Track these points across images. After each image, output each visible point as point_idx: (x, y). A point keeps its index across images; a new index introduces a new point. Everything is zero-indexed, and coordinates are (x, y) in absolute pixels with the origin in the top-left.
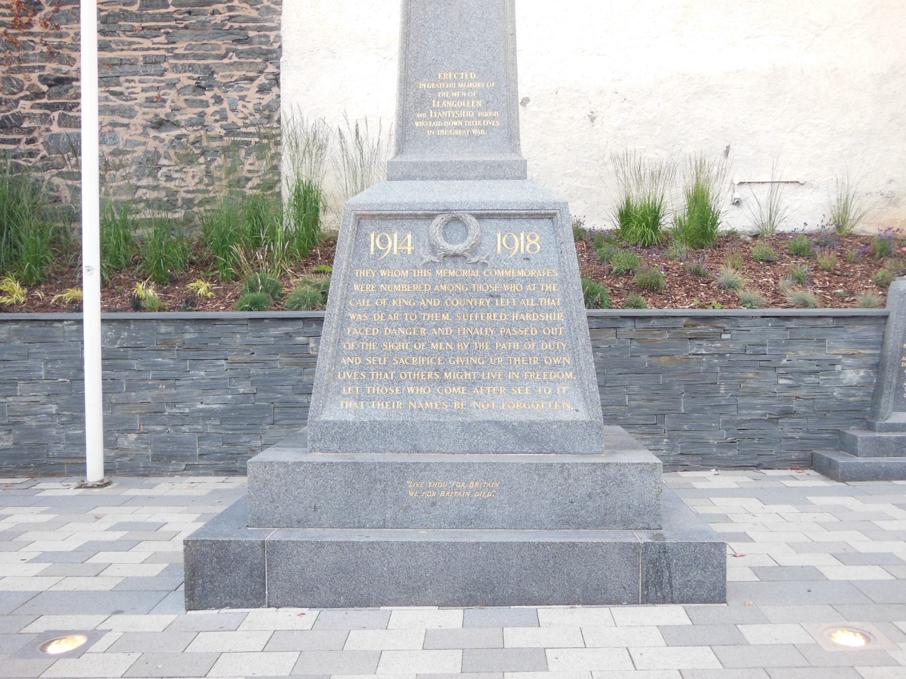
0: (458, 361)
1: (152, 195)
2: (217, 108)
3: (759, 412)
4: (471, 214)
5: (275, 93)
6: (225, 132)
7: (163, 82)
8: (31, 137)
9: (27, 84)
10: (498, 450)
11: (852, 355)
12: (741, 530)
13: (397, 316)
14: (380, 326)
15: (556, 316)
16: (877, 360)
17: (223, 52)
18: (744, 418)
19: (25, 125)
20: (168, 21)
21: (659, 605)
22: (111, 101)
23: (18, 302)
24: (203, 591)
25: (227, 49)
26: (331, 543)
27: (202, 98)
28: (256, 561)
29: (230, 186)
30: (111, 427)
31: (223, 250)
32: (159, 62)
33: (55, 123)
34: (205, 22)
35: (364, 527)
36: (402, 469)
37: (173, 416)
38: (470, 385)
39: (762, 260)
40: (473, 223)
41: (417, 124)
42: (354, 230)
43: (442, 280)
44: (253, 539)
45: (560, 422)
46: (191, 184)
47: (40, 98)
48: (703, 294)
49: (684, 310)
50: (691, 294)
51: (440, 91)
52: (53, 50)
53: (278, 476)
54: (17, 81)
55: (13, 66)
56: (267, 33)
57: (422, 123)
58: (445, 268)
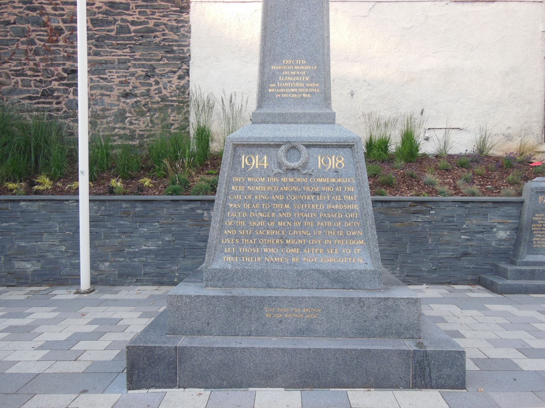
0: (294, 232)
1: (122, 132)
2: (156, 87)
4: (302, 144)
5: (187, 80)
6: (160, 99)
7: (128, 73)
8: (58, 101)
9: (56, 73)
10: (319, 287)
12: (455, 329)
14: (247, 211)
15: (354, 206)
16: (517, 226)
17: (160, 57)
18: (442, 256)
19: (55, 94)
21: (423, 390)
22: (101, 82)
23: (47, 189)
24: (138, 378)
25: (162, 56)
26: (218, 348)
27: (149, 81)
28: (171, 359)
29: (163, 128)
31: (158, 161)
32: (126, 63)
33: (71, 94)
35: (238, 335)
36: (262, 300)
37: (129, 253)
39: (443, 169)
41: (270, 90)
42: (232, 153)
44: (170, 346)
45: (356, 270)
46: (143, 126)
47: (63, 81)
48: (416, 188)
51: (284, 71)
53: (185, 304)
55: (48, 63)
57: (273, 90)
58: (287, 177)
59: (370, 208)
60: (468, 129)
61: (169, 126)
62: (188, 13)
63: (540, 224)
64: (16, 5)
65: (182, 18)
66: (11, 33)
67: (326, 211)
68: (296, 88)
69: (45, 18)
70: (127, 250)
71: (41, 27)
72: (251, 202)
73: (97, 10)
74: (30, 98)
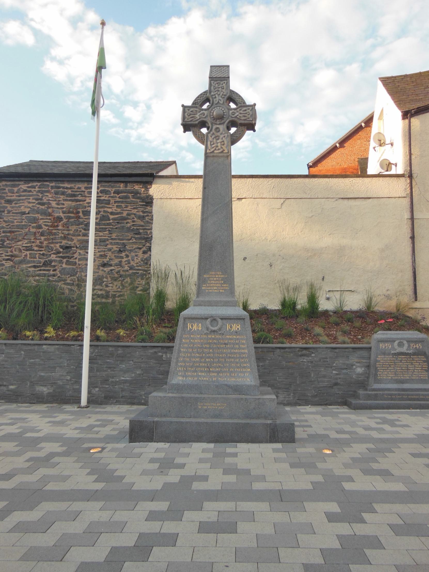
1: (100, 293)
3: (326, 384)
7: (106, 249)
9: (55, 248)
11: (359, 362)
13: (196, 350)
14: (191, 353)
17: (130, 238)
19: (53, 264)
20: (110, 226)
23: (53, 336)
29: (131, 289)
30: (91, 385)
32: (105, 241)
33: (64, 264)
34: (123, 226)
36: (196, 399)
37: (112, 382)
38: (218, 372)
40: (220, 321)
43: (210, 339)
49: (300, 345)
50: (303, 338)
52: (66, 236)
53: (158, 401)
54: (51, 247)
56: (147, 231)
57: (205, 288)
59: (253, 351)
60: (358, 291)
61: (135, 288)
62: (151, 206)
63: (382, 362)
64: (30, 201)
65: (147, 210)
66: (26, 220)
67: (231, 353)
68: (216, 287)
69: (50, 210)
70: (111, 380)
71: (47, 216)
72: (192, 348)
73: (87, 205)
74: (35, 267)
